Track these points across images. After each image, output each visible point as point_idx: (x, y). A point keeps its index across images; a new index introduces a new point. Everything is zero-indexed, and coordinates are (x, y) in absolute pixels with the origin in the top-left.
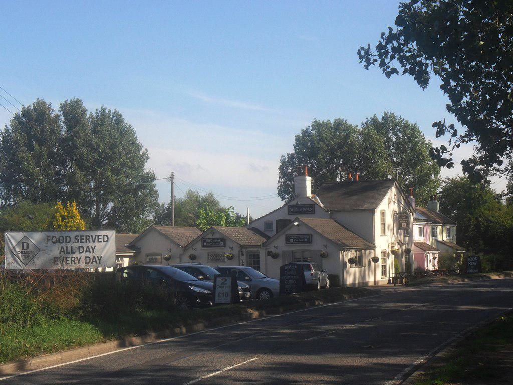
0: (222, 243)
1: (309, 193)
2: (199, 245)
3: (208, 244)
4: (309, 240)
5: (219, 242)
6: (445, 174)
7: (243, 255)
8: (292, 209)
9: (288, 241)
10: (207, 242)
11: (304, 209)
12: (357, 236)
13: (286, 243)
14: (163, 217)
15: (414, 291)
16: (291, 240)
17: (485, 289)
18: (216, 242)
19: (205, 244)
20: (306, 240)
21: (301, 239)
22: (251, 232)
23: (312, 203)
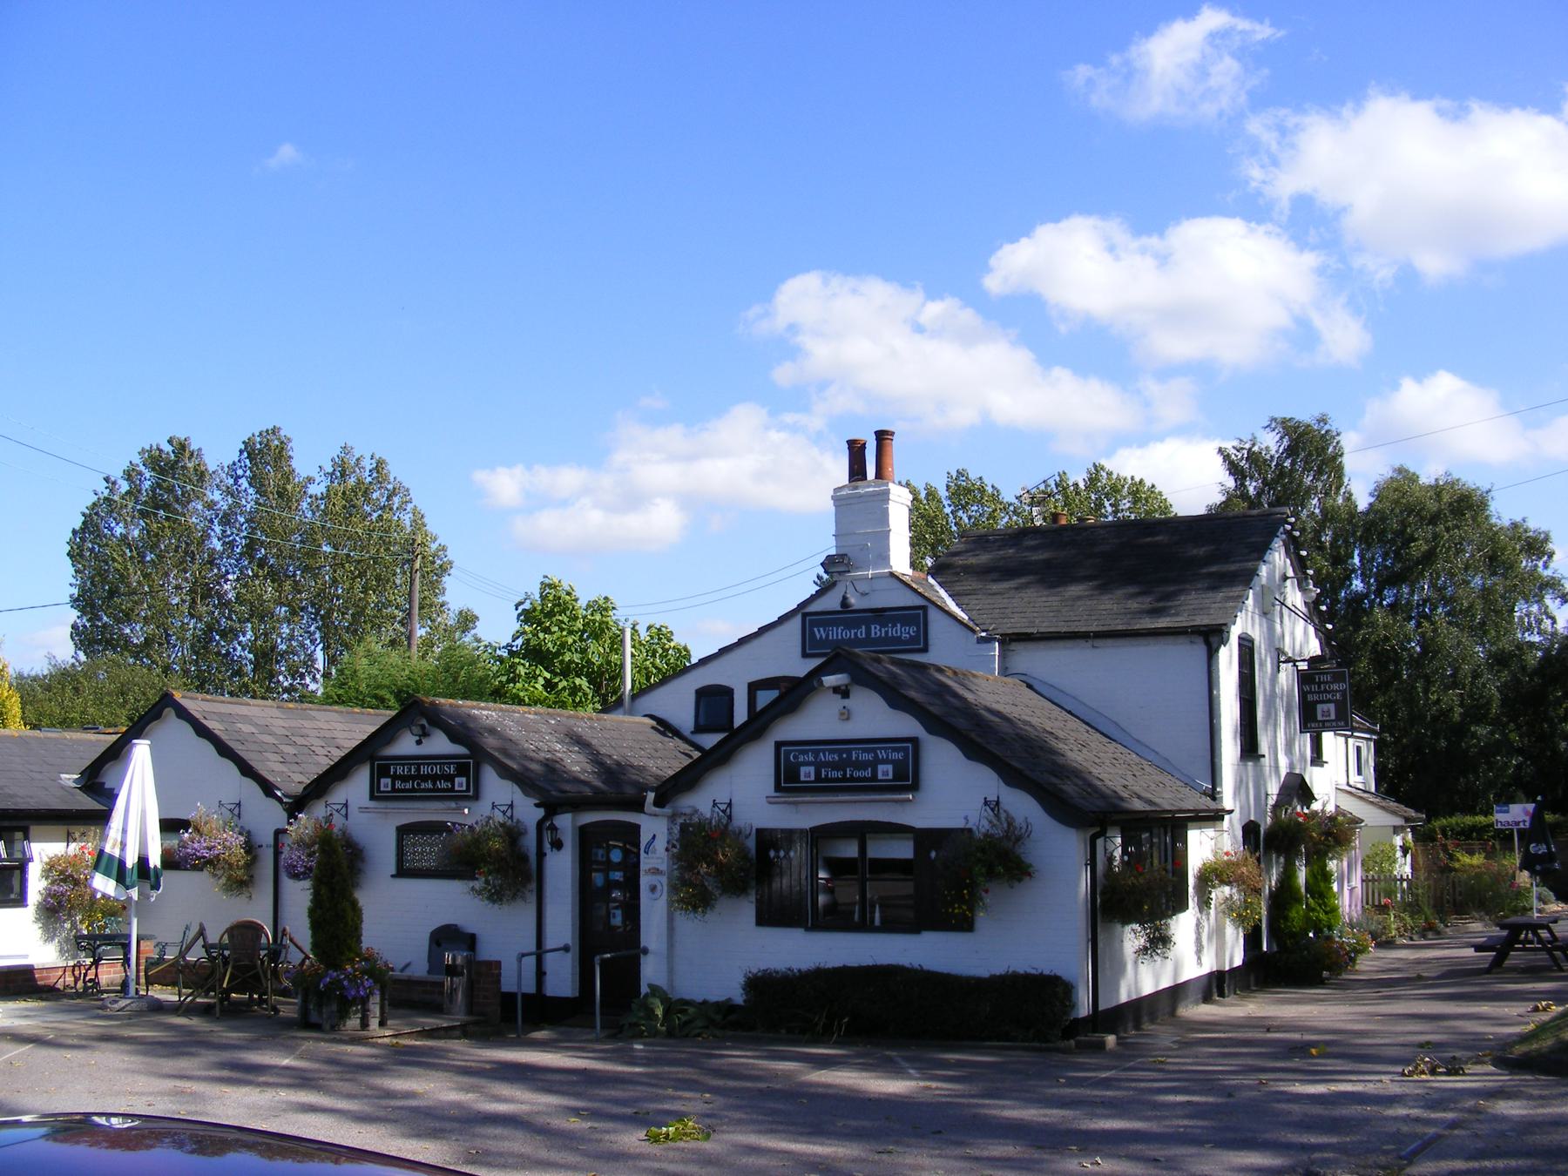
0: (460, 782)
1: (900, 558)
2: (356, 788)
3: (398, 785)
4: (900, 774)
5: (450, 778)
6: (1236, 897)
7: (557, 845)
8: (820, 633)
9: (787, 781)
10: (395, 778)
11: (876, 631)
12: (1137, 759)
13: (778, 788)
14: (212, 639)
15: (1206, 1103)
16: (807, 773)
17: (1501, 1164)
18: (434, 778)
19: (386, 783)
20: (885, 771)
21: (862, 765)
22: (1220, 459)
23: (910, 600)
